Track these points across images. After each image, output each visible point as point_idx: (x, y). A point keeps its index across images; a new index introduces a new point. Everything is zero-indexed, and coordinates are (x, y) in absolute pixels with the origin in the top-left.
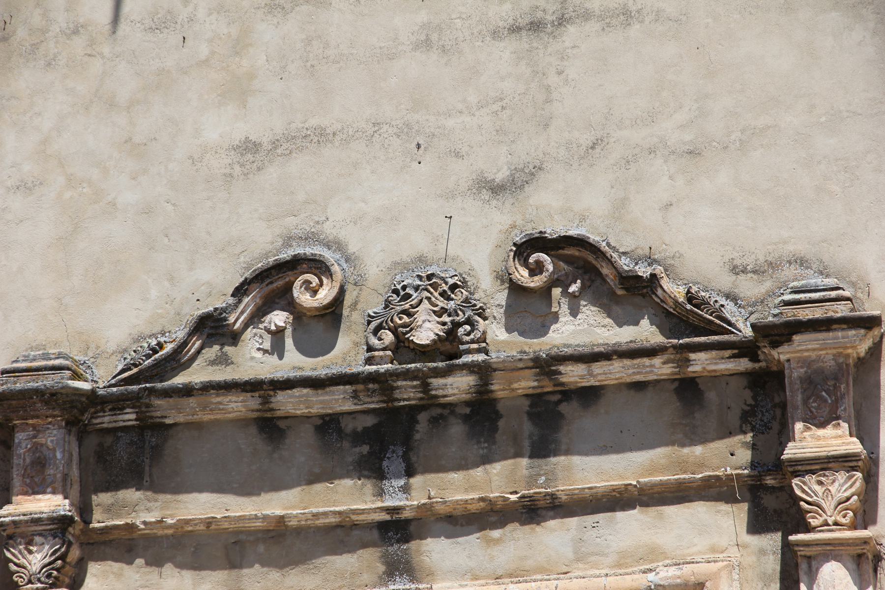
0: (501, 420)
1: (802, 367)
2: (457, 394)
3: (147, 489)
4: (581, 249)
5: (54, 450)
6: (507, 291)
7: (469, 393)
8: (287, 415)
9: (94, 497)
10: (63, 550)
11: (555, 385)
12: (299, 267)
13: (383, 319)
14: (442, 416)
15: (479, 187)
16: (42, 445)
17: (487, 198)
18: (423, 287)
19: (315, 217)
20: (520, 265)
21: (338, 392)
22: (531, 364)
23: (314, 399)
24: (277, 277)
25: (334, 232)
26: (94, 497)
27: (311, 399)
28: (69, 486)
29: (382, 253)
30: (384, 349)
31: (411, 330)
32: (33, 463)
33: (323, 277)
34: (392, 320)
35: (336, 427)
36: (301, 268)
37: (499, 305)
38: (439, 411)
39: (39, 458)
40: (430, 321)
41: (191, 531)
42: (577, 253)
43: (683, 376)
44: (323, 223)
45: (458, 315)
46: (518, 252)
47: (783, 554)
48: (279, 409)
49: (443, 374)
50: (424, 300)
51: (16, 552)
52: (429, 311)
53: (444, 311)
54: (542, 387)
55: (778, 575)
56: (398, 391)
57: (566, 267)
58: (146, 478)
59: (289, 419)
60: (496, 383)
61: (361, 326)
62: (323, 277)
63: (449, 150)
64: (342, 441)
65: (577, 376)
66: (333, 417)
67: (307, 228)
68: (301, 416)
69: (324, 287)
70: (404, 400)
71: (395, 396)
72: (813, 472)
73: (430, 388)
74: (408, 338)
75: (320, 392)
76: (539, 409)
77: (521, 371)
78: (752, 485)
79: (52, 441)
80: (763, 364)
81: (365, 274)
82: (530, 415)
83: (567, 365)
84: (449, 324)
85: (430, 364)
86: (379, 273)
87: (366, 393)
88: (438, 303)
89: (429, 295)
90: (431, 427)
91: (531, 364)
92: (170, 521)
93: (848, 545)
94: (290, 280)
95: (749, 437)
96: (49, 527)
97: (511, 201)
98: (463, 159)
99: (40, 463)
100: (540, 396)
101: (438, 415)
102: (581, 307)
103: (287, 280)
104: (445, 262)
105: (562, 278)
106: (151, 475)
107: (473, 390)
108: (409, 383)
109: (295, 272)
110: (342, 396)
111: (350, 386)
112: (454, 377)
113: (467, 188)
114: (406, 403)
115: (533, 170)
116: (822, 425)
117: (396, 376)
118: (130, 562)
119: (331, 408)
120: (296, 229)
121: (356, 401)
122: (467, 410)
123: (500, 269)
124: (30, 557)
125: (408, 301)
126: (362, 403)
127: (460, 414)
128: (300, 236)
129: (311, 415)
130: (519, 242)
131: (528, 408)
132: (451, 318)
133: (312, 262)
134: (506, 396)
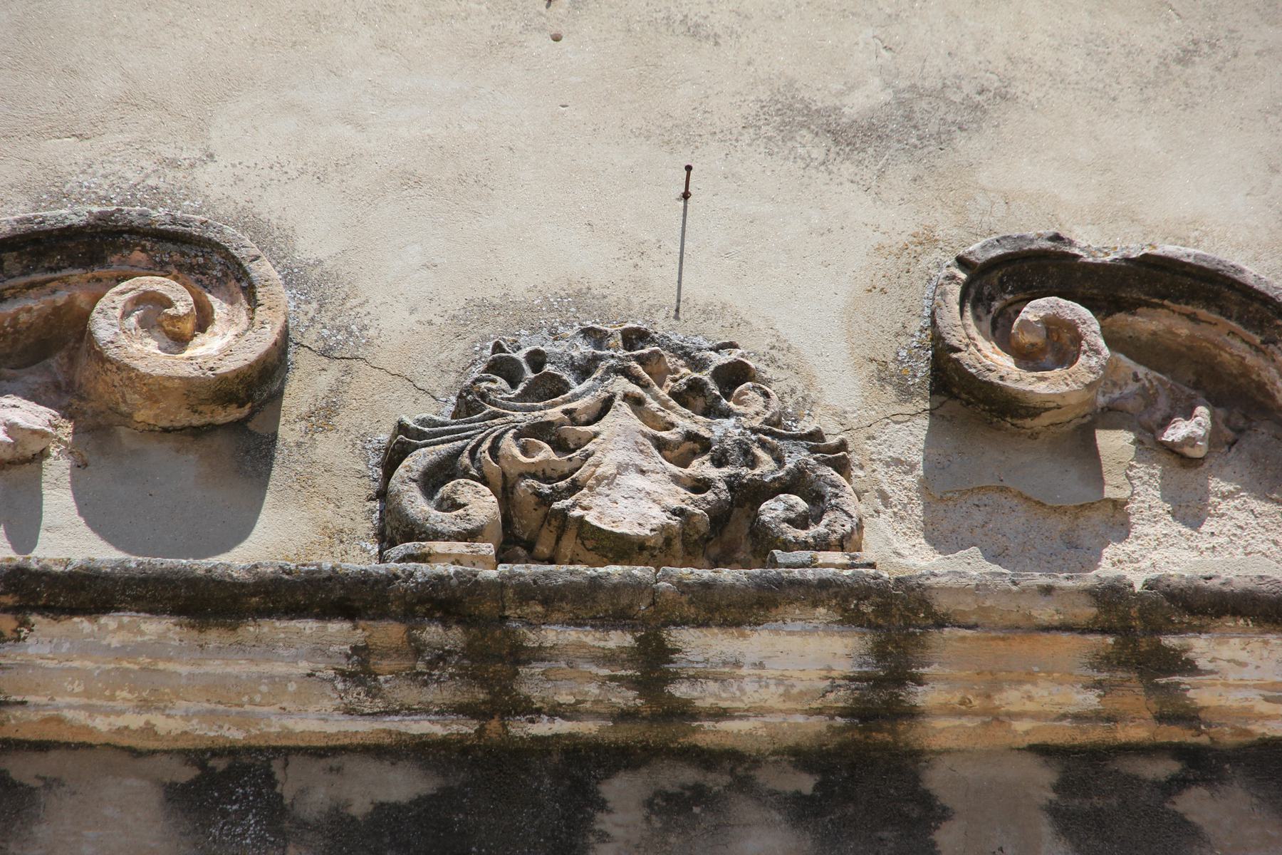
0: (945, 826)
2: (771, 711)
4: (1202, 312)
6: (924, 422)
7: (819, 712)
8: (50, 734)
11: (1161, 718)
12: (115, 258)
13: (460, 443)
14: (699, 794)
15: (784, 123)
17: (818, 154)
18: (612, 361)
19: (161, 148)
20: (981, 332)
21: (289, 646)
22: (1087, 612)
23: (184, 670)
24: (22, 281)
25: (239, 196)
27: (171, 667)
29: (425, 273)
30: (470, 536)
31: (575, 487)
33: (210, 297)
34: (494, 450)
35: (258, 794)
36: (122, 263)
37: (898, 462)
38: (689, 775)
40: (643, 472)
42: (1184, 329)
44: (192, 166)
45: (753, 462)
46: (972, 291)
48: (23, 703)
49: (733, 613)
50: (617, 402)
52: (641, 439)
53: (698, 445)
54: (1111, 719)
56: (538, 668)
57: (1142, 371)
59: (53, 754)
60: (936, 679)
61: (354, 481)
62: (210, 297)
63: (661, 15)
64: (284, 847)
65: (1255, 687)
66: (246, 760)
67: (129, 175)
68: (107, 745)
69: (217, 327)
70: (556, 711)
71: (524, 690)
73: (672, 667)
74: (563, 513)
75: (214, 637)
76: (1098, 802)
77: (1046, 637)
81: (364, 328)
82: (1063, 819)
83: (1224, 637)
84: (722, 485)
85: (685, 570)
86: (417, 327)
87: (407, 664)
88: (673, 417)
89: (638, 390)
90: (658, 824)
91: (1087, 612)
94: (70, 303)
97: (909, 170)
98: (716, 44)
100: (1096, 756)
101: (683, 787)
102: (1213, 499)
103: (61, 298)
104: (677, 318)
105: (1130, 405)
107: (839, 698)
108: (590, 638)
109: (98, 272)
110: (304, 667)
111: (347, 625)
112: (776, 632)
113: (741, 123)
114: (562, 727)
115: (978, 98)
117: (546, 602)
119: (243, 721)
120: (84, 172)
121: (356, 695)
122: (806, 783)
123: (891, 356)
125: (559, 399)
126: (379, 704)
127: (773, 793)
128: (102, 193)
129: (151, 745)
130: (981, 257)
131: (1052, 796)
132: (727, 470)
133: (170, 245)
134: (962, 743)
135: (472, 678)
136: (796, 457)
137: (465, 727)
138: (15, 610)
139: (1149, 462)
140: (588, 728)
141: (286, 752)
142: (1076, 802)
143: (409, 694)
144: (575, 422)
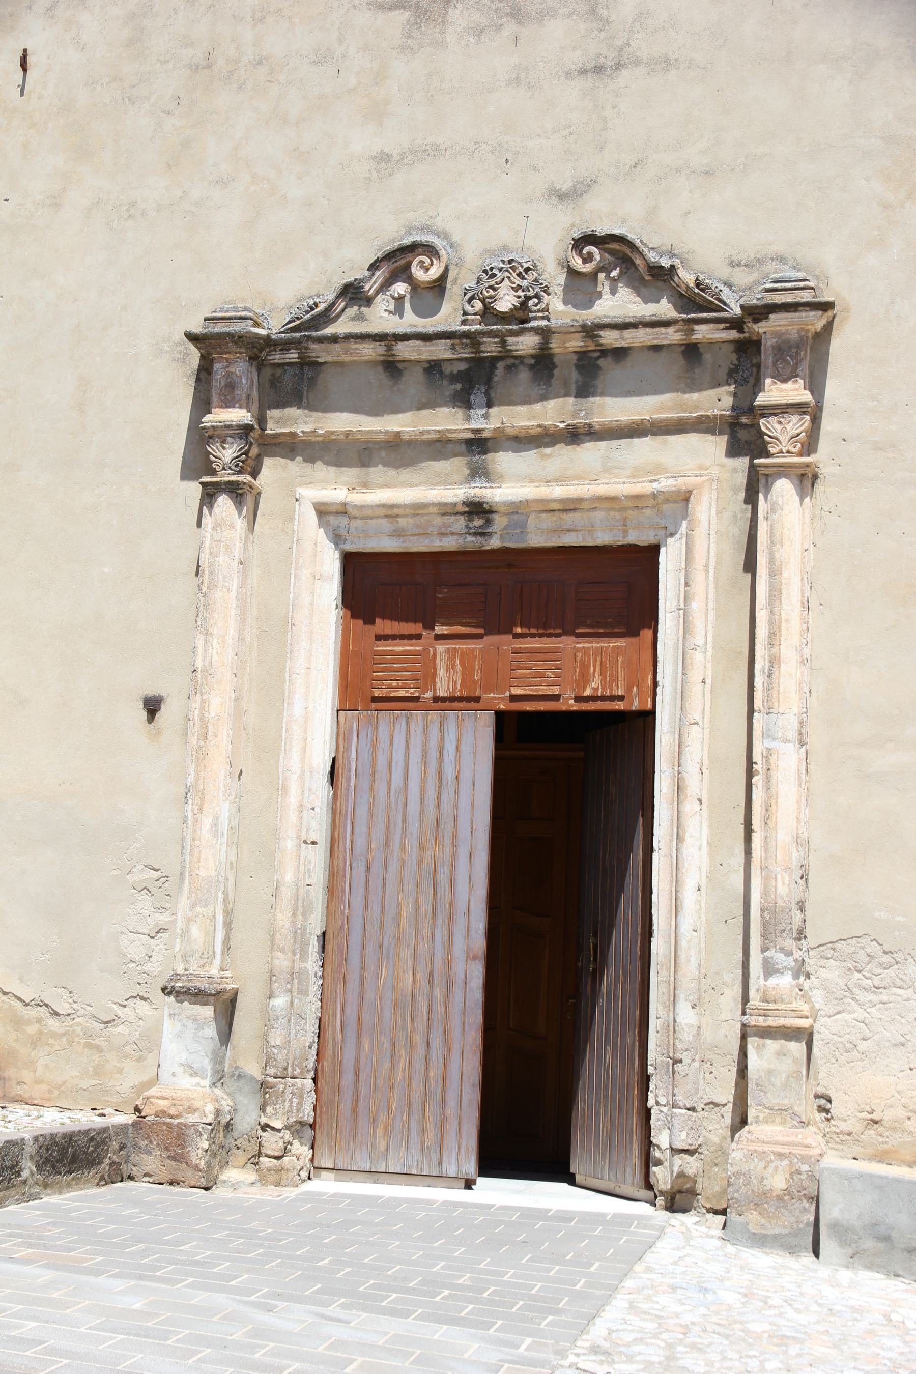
1: (774, 338)
3: (305, 408)
5: (241, 377)
6: (565, 274)
9: (268, 412)
10: (246, 448)
11: (596, 346)
14: (514, 365)
16: (232, 373)
26: (268, 412)
28: (251, 403)
30: (475, 314)
32: (226, 386)
34: (481, 293)
39: (230, 382)
41: (335, 440)
42: (618, 248)
43: (688, 342)
45: (529, 291)
47: (749, 472)
51: (215, 448)
54: (587, 346)
55: (744, 487)
58: (305, 400)
70: (488, 352)
72: (775, 415)
78: (732, 423)
79: (239, 371)
80: (747, 335)
82: (578, 367)
83: (606, 331)
88: (516, 281)
91: (580, 329)
92: (320, 432)
93: (796, 467)
95: (732, 388)
96: (237, 432)
97: (573, 205)
99: (231, 386)
100: (585, 352)
103: (408, 260)
106: (307, 398)
108: (491, 340)
116: (785, 381)
118: (293, 459)
121: (453, 351)
124: (224, 452)
130: (576, 238)
132: (524, 293)
135: (473, 347)
136: (537, 289)
137: (474, 355)
138: (395, 341)
139: (607, 280)
140: (494, 354)
141: (444, 360)
142: (230, 641)
143: (462, 351)
144: (497, 284)
